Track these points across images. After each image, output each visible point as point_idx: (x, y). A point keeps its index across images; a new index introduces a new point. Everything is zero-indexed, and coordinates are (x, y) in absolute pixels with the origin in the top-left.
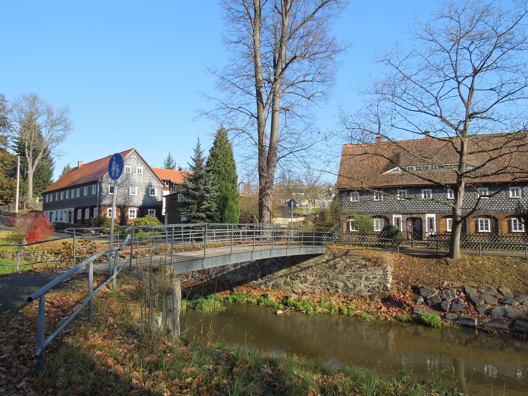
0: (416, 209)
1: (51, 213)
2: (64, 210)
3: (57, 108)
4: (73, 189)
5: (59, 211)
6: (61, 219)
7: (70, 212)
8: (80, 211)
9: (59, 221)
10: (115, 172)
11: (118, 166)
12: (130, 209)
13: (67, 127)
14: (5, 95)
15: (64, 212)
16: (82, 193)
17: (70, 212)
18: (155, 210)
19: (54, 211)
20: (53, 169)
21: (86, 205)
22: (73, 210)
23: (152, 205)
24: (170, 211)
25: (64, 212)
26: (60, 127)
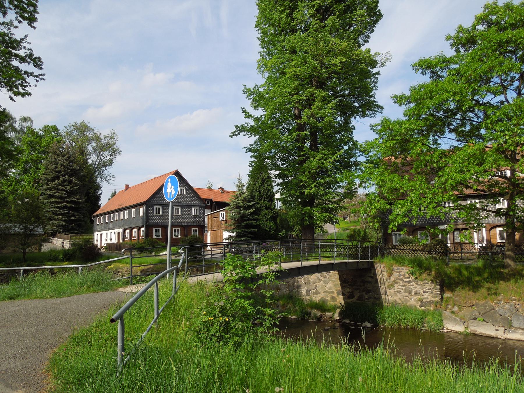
0: (431, 221)
1: (101, 234)
2: (112, 231)
3: (104, 132)
4: (122, 211)
5: (109, 232)
6: (111, 240)
7: (119, 233)
8: (128, 231)
9: (109, 241)
10: (171, 193)
11: (173, 187)
12: (154, 229)
13: (114, 152)
14: (46, 124)
15: (113, 233)
16: (130, 214)
17: (119, 233)
18: (179, 229)
19: (104, 233)
20: (101, 194)
21: (133, 226)
22: (121, 230)
23: (195, 224)
24: (212, 230)
25: (113, 233)
26: (107, 153)
